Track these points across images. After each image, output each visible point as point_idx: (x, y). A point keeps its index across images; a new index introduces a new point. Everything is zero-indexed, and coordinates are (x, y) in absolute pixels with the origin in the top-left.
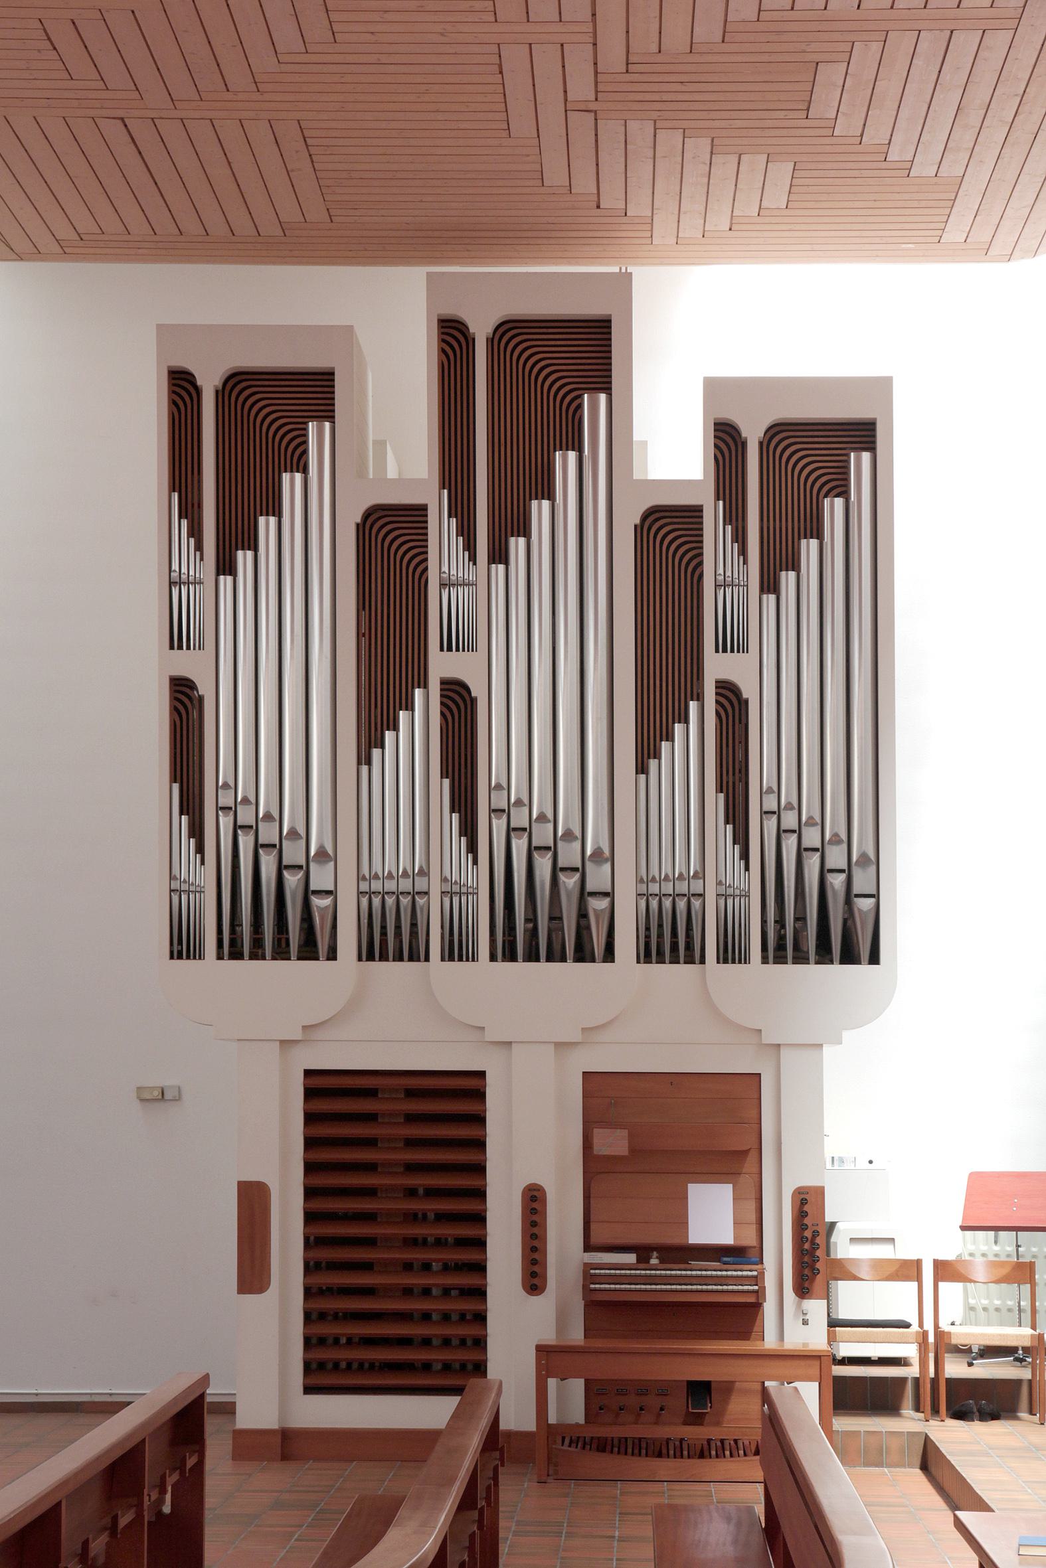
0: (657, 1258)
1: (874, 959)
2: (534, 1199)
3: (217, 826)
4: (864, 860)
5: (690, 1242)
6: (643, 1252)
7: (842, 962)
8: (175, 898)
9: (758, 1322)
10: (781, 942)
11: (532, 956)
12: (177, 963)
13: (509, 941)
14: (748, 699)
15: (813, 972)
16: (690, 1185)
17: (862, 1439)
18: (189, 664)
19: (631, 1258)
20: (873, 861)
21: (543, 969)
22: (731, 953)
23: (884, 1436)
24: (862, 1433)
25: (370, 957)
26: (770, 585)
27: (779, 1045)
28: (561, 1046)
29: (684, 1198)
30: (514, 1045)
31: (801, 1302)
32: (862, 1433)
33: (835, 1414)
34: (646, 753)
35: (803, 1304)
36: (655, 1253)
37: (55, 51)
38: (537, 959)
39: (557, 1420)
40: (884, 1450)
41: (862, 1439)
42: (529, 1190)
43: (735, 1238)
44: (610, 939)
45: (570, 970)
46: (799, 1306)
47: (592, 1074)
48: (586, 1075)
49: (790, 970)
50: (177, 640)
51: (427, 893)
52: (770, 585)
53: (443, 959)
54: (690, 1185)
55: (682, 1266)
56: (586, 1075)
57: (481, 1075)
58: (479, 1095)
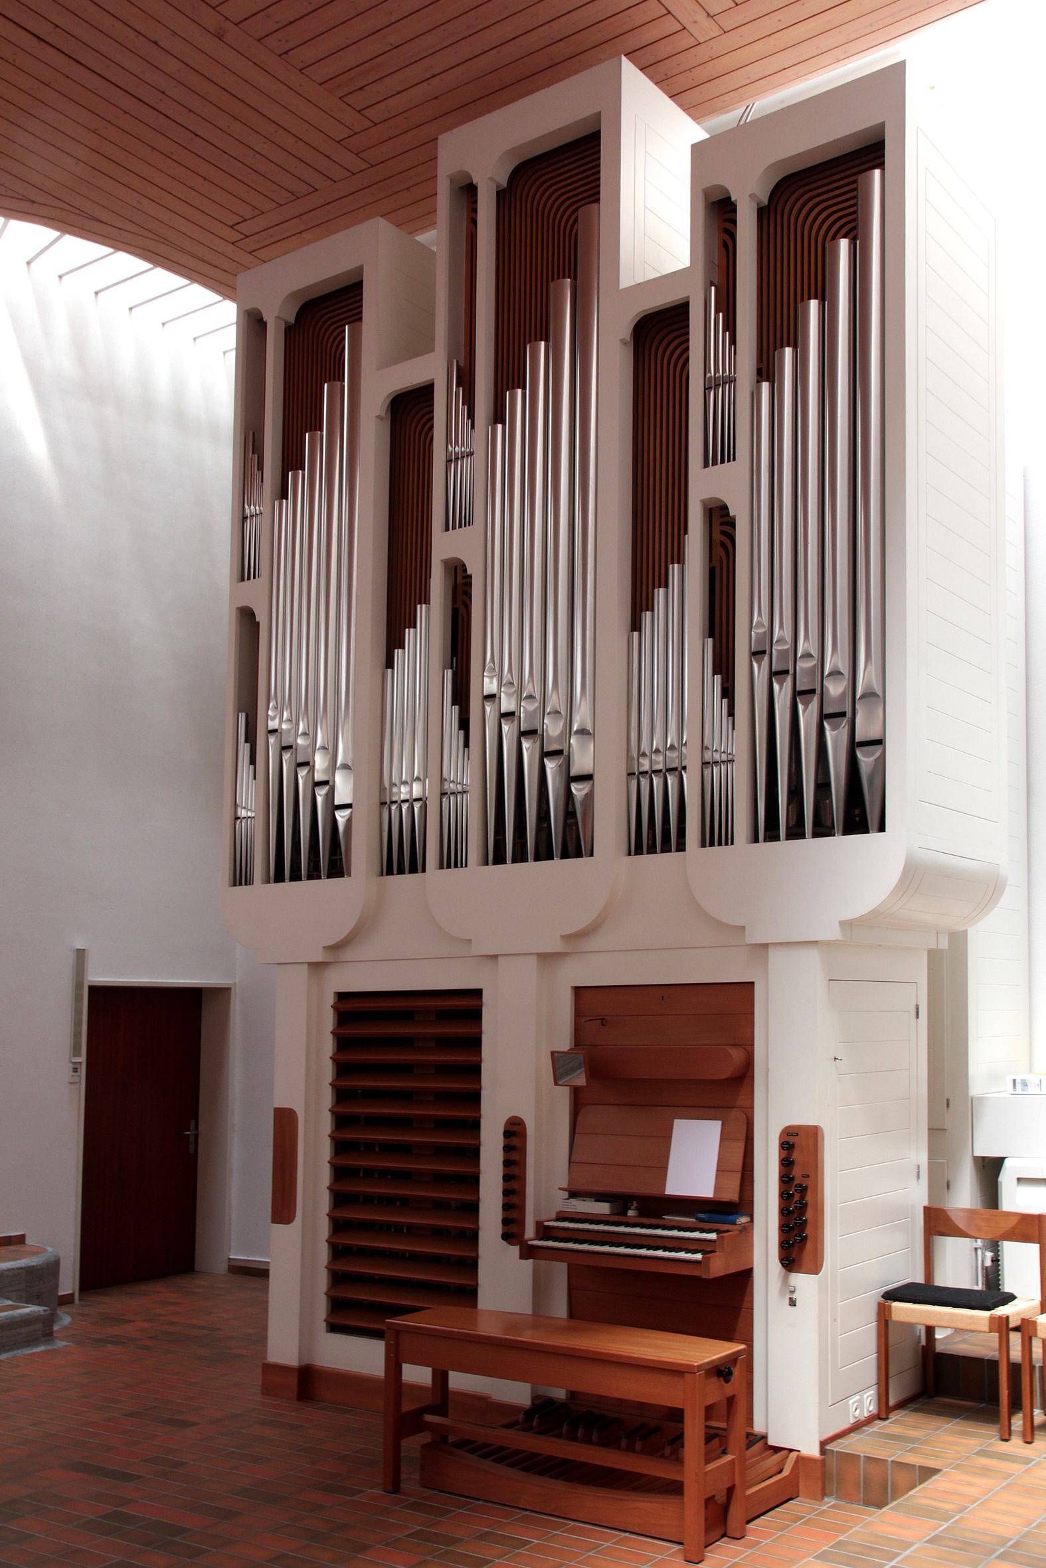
0: (636, 1209)
1: (882, 828)
2: (514, 1132)
3: (484, 716)
4: (869, 695)
5: (666, 1193)
6: (621, 1202)
7: (816, 834)
8: (707, 772)
9: (747, 1298)
10: (333, 858)
11: (544, 853)
12: (709, 850)
13: (336, 855)
14: (735, 516)
15: (811, 847)
16: (677, 1122)
17: (862, 1466)
18: (254, 594)
19: (603, 1208)
20: (876, 697)
21: (532, 869)
22: (452, 859)
23: (889, 1467)
24: (862, 1459)
25: (638, 851)
26: (766, 370)
27: (766, 946)
28: (546, 959)
29: (667, 1138)
30: (500, 958)
31: (789, 1275)
32: (862, 1459)
33: (567, 1391)
34: (640, 603)
35: (790, 1277)
36: (634, 1203)
37: (228, 21)
38: (550, 857)
39: (300, 1360)
40: (889, 1487)
41: (862, 1466)
42: (511, 1124)
43: (716, 1189)
44: (666, 827)
45: (558, 866)
46: (785, 1281)
47: (715, 986)
48: (578, 991)
49: (785, 847)
50: (245, 571)
51: (879, 742)
52: (766, 370)
53: (703, 845)
54: (677, 1122)
55: (654, 1221)
56: (578, 991)
57: (477, 993)
58: (475, 1015)
